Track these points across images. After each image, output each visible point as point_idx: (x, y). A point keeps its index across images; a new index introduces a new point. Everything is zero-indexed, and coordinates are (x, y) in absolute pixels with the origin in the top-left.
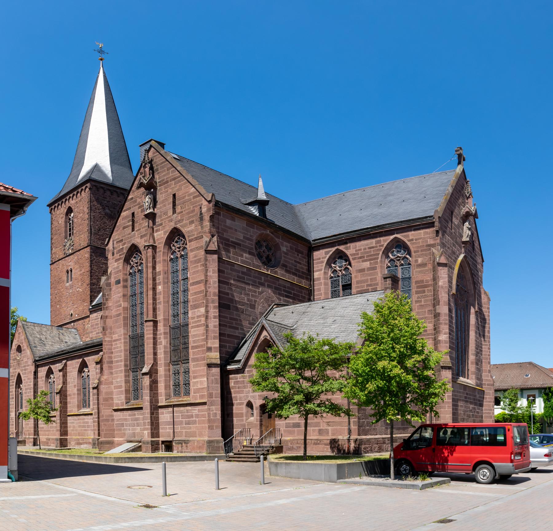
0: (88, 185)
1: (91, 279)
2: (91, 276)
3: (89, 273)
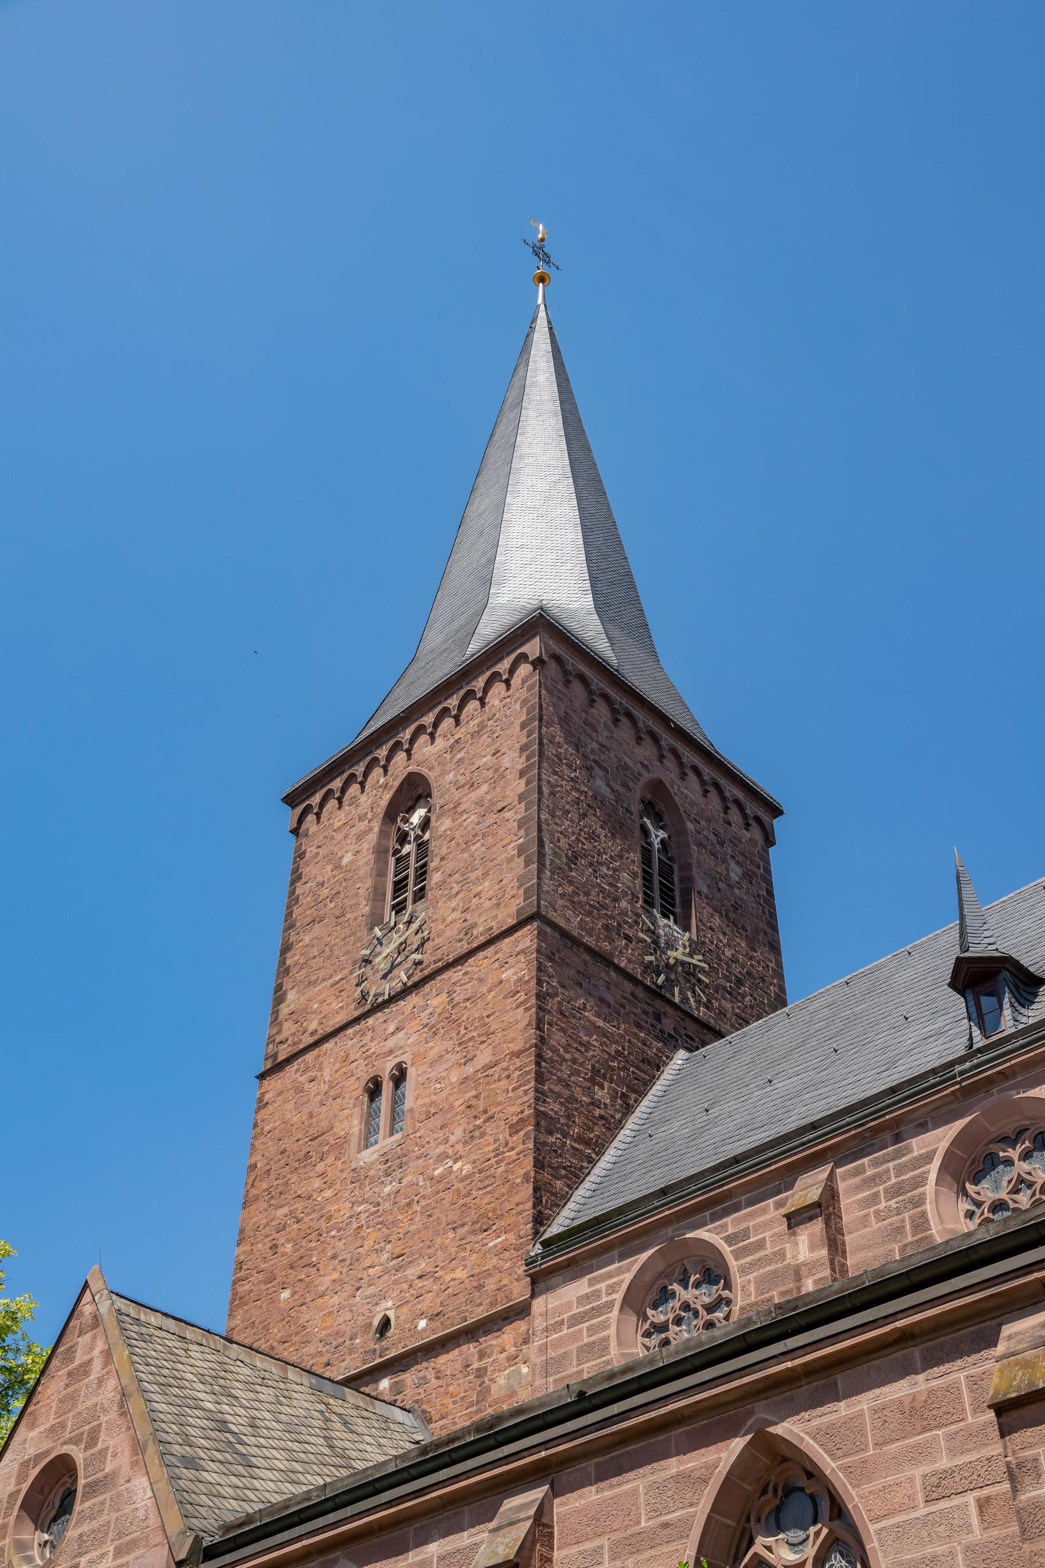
1: (540, 1096)
2: (540, 1078)
3: (529, 1059)
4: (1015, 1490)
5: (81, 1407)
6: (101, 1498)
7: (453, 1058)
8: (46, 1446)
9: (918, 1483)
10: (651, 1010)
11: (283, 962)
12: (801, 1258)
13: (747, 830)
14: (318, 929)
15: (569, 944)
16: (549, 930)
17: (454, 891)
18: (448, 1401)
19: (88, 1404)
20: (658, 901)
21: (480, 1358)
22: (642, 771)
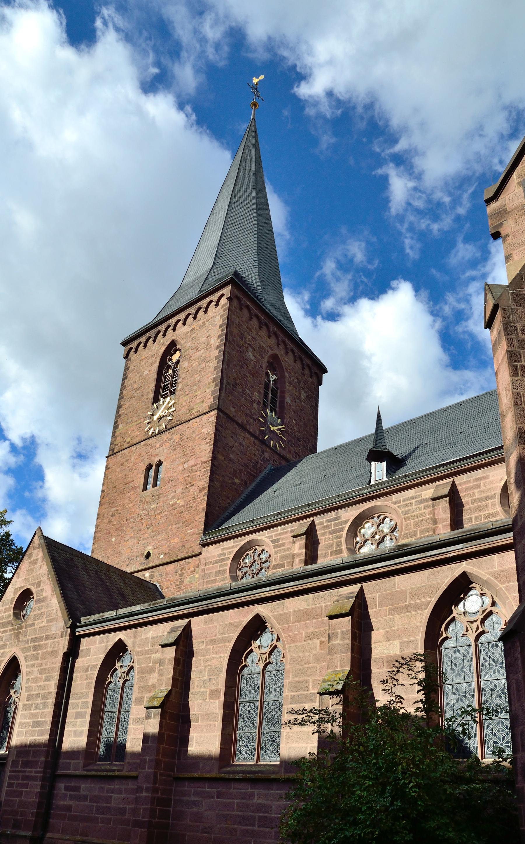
0: (227, 291)
4: (329, 641)
5: (34, 574)
6: (42, 604)
7: (181, 460)
8: (23, 585)
9: (304, 635)
10: (260, 449)
11: (118, 412)
12: (295, 552)
13: (311, 378)
14: (133, 401)
15: (230, 421)
16: (222, 415)
17: (186, 393)
18: (169, 583)
19: (37, 573)
20: (270, 405)
21: (181, 571)
22: (269, 350)
